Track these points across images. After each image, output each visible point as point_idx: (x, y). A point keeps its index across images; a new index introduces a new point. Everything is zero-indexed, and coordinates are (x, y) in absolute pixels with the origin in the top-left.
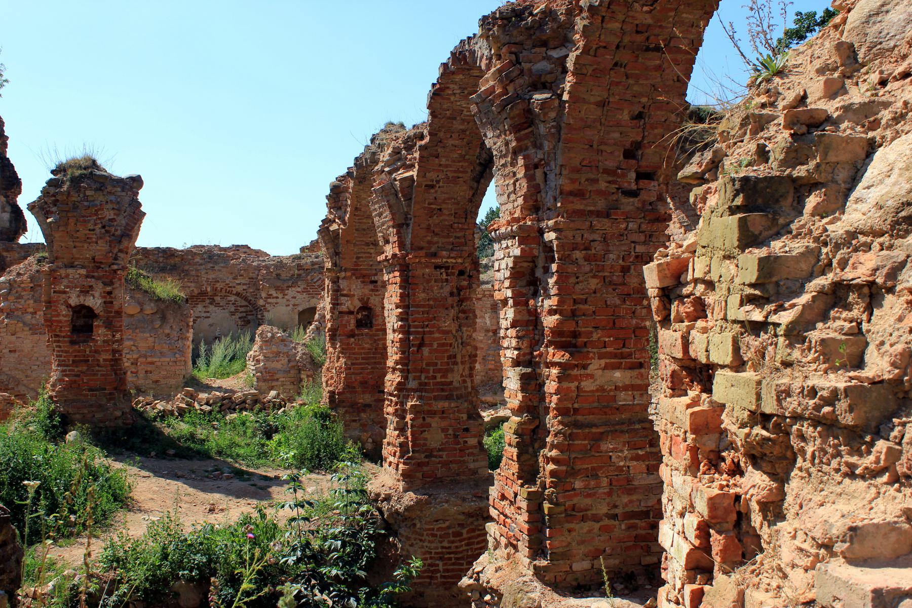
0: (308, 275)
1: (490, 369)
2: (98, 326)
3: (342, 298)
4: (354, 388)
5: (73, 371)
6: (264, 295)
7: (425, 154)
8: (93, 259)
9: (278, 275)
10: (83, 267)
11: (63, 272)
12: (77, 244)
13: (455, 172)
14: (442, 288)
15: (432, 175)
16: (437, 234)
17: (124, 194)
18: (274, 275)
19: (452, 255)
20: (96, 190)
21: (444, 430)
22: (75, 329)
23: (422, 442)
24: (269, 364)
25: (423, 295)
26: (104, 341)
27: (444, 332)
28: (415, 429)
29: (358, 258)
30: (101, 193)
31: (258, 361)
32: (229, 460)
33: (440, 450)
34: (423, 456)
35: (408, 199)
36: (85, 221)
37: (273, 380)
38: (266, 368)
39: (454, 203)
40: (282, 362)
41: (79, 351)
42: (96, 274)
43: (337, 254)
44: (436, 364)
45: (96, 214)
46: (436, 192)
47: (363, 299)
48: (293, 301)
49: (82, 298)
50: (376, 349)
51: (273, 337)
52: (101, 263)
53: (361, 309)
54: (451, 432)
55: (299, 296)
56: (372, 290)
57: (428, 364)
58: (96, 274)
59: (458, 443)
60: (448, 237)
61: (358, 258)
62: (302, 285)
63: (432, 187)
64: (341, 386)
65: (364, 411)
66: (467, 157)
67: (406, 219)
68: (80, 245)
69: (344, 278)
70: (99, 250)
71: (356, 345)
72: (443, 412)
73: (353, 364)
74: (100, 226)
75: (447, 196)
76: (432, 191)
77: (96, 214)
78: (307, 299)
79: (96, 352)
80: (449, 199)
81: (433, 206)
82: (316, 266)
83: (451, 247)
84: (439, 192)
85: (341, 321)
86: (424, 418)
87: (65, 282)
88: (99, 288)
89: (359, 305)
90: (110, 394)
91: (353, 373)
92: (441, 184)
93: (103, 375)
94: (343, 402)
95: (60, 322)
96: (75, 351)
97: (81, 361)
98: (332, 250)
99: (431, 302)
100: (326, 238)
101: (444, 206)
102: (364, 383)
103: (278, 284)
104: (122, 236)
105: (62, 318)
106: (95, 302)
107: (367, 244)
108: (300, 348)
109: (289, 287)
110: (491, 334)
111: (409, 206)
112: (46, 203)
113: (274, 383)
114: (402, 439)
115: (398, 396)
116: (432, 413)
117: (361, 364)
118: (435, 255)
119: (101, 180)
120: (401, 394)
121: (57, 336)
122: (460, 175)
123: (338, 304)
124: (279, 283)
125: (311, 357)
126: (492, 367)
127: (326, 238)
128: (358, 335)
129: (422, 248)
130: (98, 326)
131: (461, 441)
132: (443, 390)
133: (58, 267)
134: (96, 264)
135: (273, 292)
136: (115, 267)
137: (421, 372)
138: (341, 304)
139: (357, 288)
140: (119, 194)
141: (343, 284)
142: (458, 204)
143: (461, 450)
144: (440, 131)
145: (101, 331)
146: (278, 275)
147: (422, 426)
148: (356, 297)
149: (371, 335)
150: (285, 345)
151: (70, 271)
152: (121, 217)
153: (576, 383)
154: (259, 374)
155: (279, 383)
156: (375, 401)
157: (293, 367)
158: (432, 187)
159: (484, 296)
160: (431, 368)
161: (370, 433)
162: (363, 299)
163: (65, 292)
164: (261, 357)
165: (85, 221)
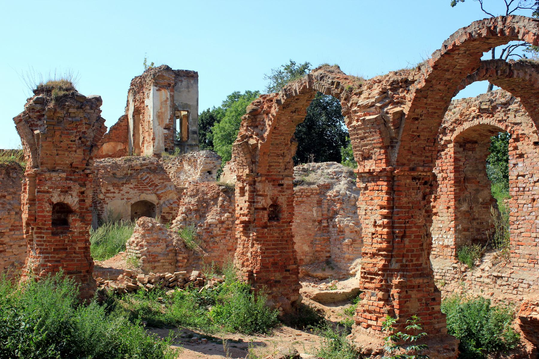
0: (138, 174)
1: (317, 251)
2: (75, 220)
3: (259, 197)
4: (268, 268)
5: (54, 257)
6: (103, 190)
7: (419, 95)
8: (71, 164)
9: (114, 174)
10: (63, 171)
11: (47, 175)
12: (60, 152)
13: (434, 108)
14: (417, 194)
15: (418, 111)
16: (414, 154)
17: (92, 111)
18: (111, 174)
19: (425, 170)
20: (78, 108)
21: (420, 300)
22: (54, 223)
23: (405, 309)
24: (151, 249)
25: (405, 200)
26: (80, 233)
27: (419, 227)
28: (401, 299)
29: (270, 166)
30: (82, 111)
31: (142, 246)
32: (190, 328)
35: (397, 127)
36: (68, 134)
37: (155, 262)
38: (148, 252)
39: (429, 132)
40: (162, 247)
41: (59, 241)
42: (73, 177)
43: (253, 163)
44: (413, 251)
45: (76, 128)
46: (419, 123)
47: (273, 198)
48: (127, 196)
49: (62, 197)
50: (282, 237)
51: (153, 226)
52: (77, 168)
53: (271, 206)
54: (424, 301)
55: (132, 191)
56: (280, 191)
57: (407, 251)
58: (73, 177)
59: (428, 309)
60: (421, 156)
61: (270, 166)
62: (134, 182)
63: (417, 119)
64: (258, 267)
65: (275, 286)
66: (445, 98)
67: (392, 142)
68: (63, 153)
69: (260, 182)
70: (77, 158)
71: (268, 234)
72: (419, 286)
73: (266, 249)
74: (78, 138)
75: (425, 126)
76: (416, 122)
77: (76, 128)
78: (138, 194)
79: (73, 241)
80: (426, 128)
81: (415, 134)
82: (144, 167)
83: (422, 164)
84: (420, 123)
85: (258, 215)
86: (407, 292)
87: (49, 183)
88: (76, 189)
89: (270, 202)
90: (85, 276)
91: (267, 257)
92: (423, 117)
93: (78, 261)
94: (260, 279)
95: (45, 216)
96: (56, 241)
97: (61, 249)
98: (249, 160)
99: (411, 205)
100: (245, 150)
101: (422, 133)
102: (275, 264)
103: (115, 182)
104: (92, 146)
105: (46, 213)
106: (72, 200)
107: (278, 156)
108: (174, 236)
109: (123, 184)
110: (317, 223)
111: (397, 133)
112: (30, 117)
113: (156, 264)
114: (388, 308)
115: (383, 275)
116: (412, 287)
117: (272, 249)
118: (413, 169)
119: (81, 100)
120: (386, 273)
121: (40, 228)
122: (437, 111)
123: (254, 202)
124: (115, 181)
125: (183, 242)
126: (318, 249)
127: (245, 150)
128: (270, 226)
129: (404, 165)
130: (75, 220)
131: (430, 307)
132: (417, 270)
133: (42, 171)
134: (73, 168)
135: (111, 188)
136: (88, 171)
137: (403, 257)
138: (257, 202)
139: (268, 190)
140: (89, 111)
141: (259, 186)
142: (431, 132)
143: (430, 315)
144: (434, 79)
145: (78, 224)
146: (114, 174)
147: (406, 297)
148: (269, 197)
149: (278, 227)
150: (163, 233)
151: (54, 174)
152: (90, 130)
154: (144, 257)
155: (160, 264)
156: (283, 278)
157: (171, 251)
158: (417, 119)
159: (312, 194)
160: (410, 254)
161: (281, 303)
162: (273, 198)
163: (48, 192)
164: (144, 243)
165: (68, 134)
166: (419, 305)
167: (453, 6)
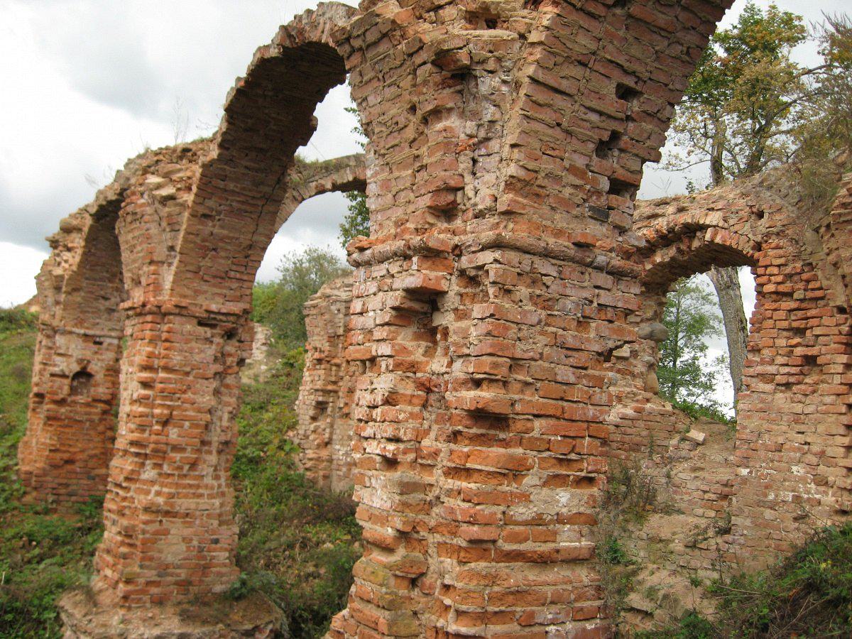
21: (186, 540)
33: (179, 567)
34: (154, 572)
54: (195, 543)
72: (187, 515)
89: (76, 368)
92: (222, 216)
153: (502, 508)
166: (185, 549)
167: (346, 109)
